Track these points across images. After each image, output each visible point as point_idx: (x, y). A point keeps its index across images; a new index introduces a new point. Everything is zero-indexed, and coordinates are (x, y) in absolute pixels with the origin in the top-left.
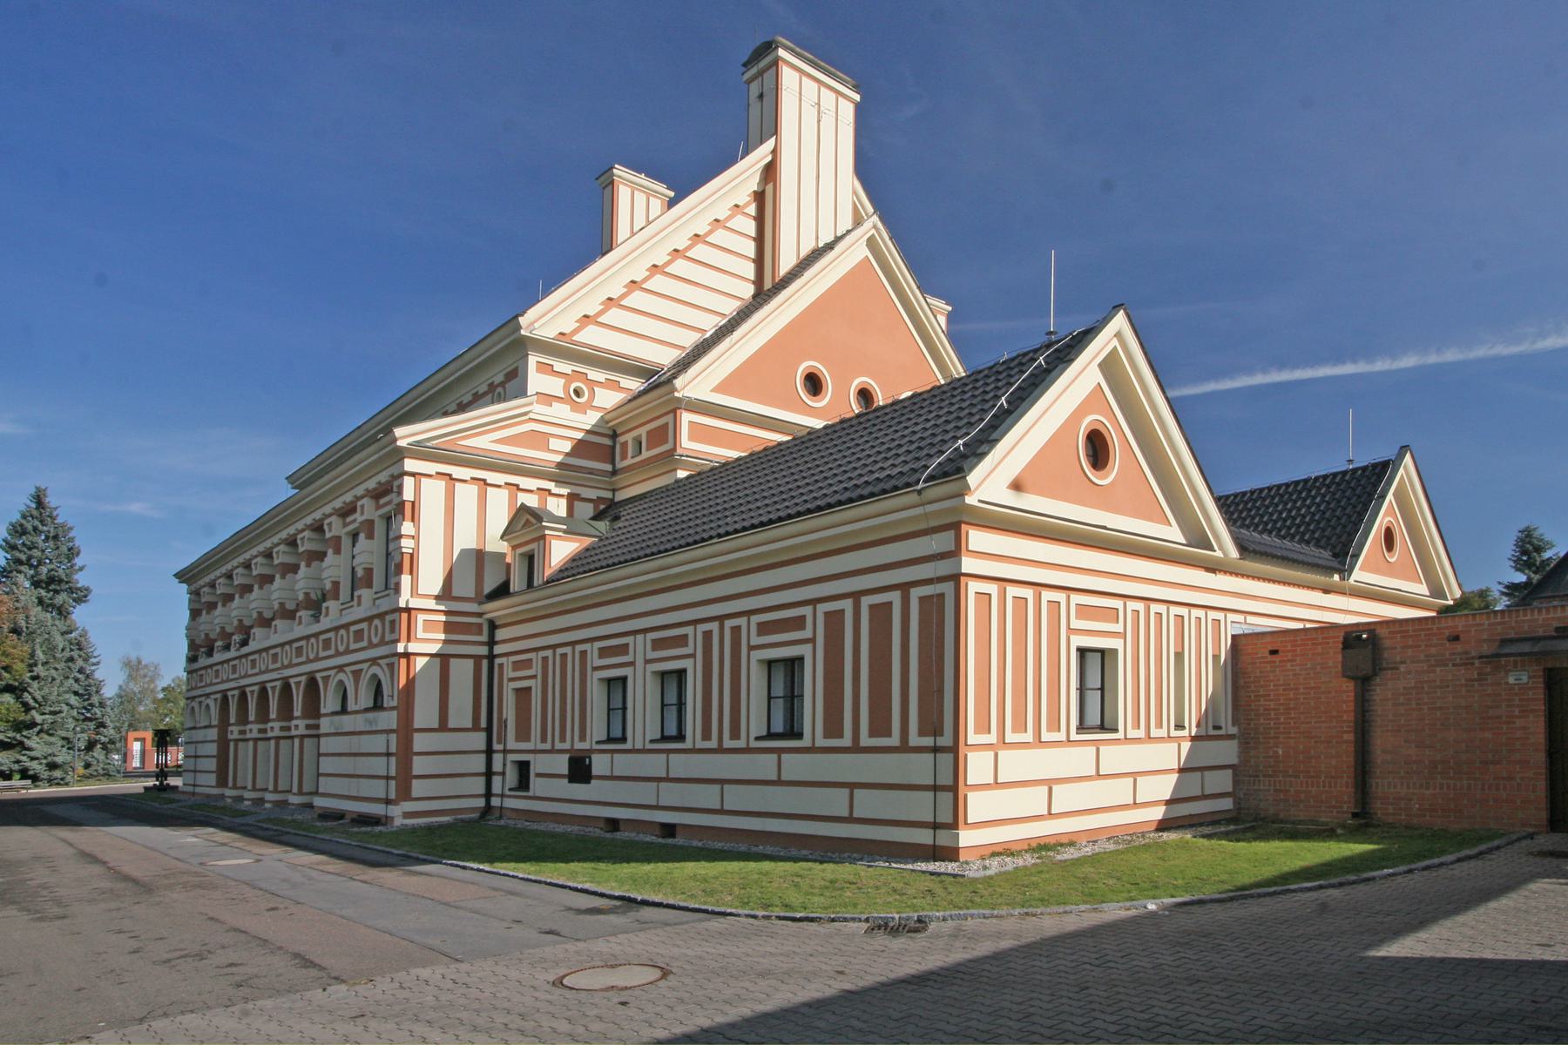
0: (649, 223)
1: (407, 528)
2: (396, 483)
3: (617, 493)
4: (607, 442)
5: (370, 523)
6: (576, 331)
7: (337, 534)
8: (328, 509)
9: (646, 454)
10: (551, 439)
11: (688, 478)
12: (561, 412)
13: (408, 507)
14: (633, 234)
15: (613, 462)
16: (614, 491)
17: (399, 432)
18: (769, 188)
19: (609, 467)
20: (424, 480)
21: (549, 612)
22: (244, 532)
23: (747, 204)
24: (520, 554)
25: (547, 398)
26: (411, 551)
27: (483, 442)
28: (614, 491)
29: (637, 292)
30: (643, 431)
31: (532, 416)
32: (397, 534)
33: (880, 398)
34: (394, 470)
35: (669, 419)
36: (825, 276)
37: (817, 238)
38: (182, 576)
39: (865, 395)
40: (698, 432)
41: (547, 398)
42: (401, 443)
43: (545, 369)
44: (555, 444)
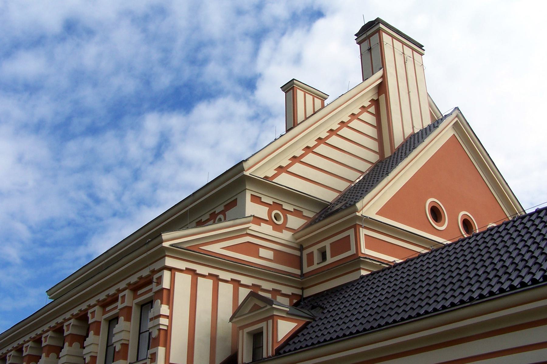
0: (315, 113)
1: (164, 309)
2: (156, 276)
3: (304, 291)
4: (297, 253)
5: (130, 308)
6: (275, 176)
7: (130, 305)
8: (93, 302)
9: (330, 260)
10: (260, 249)
11: (367, 276)
12: (266, 229)
13: (165, 293)
14: (306, 118)
15: (301, 268)
16: (303, 289)
17: (165, 236)
18: (382, 98)
19: (298, 272)
20: (177, 274)
21: (398, 352)
22: (45, 309)
23: (369, 106)
24: (248, 333)
25: (258, 220)
26: (165, 328)
27: (216, 248)
28: (303, 289)
29: (355, 120)
30: (327, 244)
31: (249, 232)
32: (156, 314)
33: (477, 228)
34: (156, 266)
35: (351, 232)
36: (428, 150)
37: (413, 127)
38: (281, 88)
39: (467, 224)
40: (372, 243)
41: (258, 220)
42: (166, 244)
43: (256, 199)
44: (263, 252)
